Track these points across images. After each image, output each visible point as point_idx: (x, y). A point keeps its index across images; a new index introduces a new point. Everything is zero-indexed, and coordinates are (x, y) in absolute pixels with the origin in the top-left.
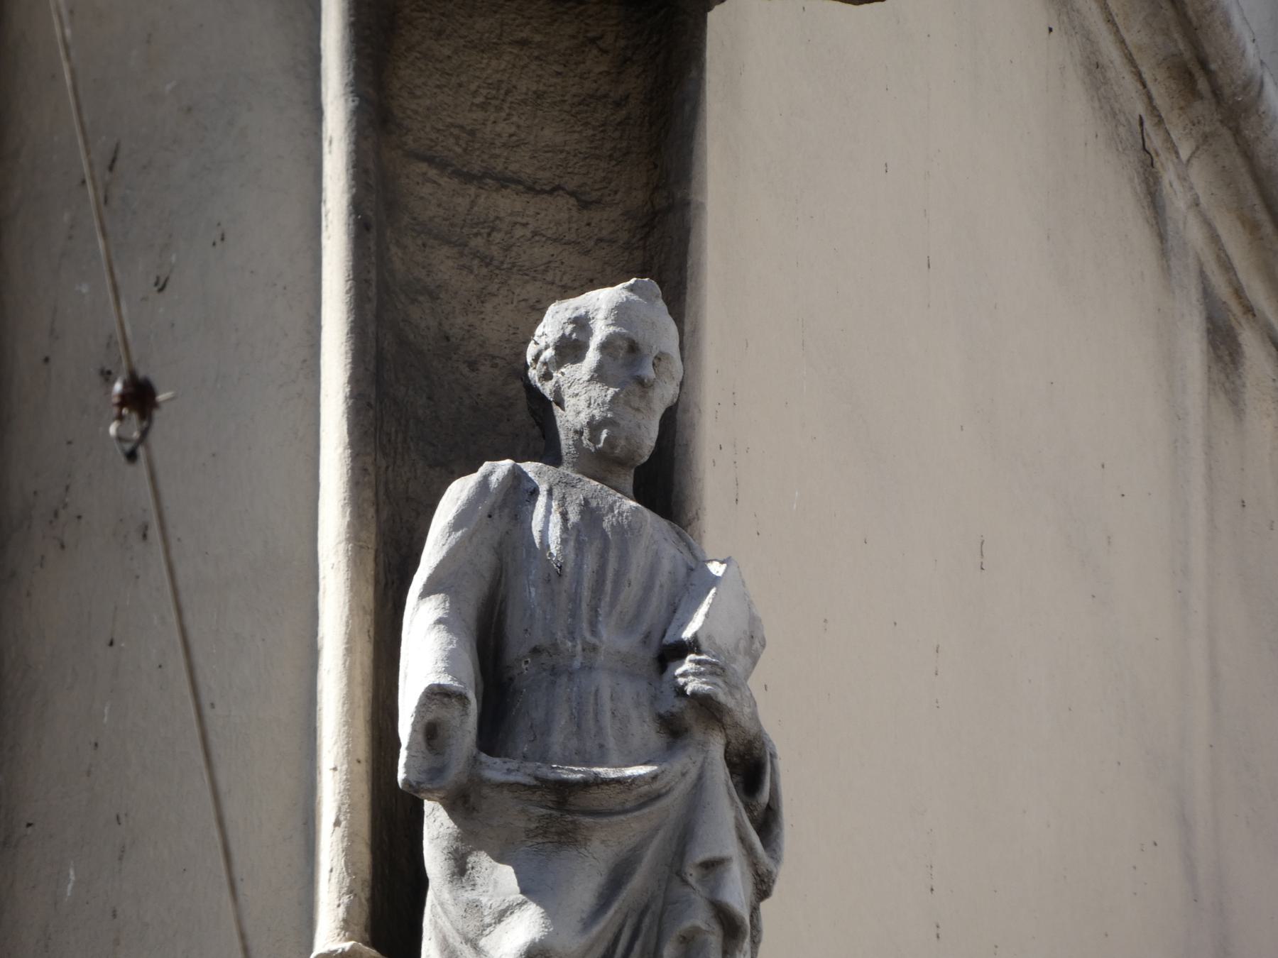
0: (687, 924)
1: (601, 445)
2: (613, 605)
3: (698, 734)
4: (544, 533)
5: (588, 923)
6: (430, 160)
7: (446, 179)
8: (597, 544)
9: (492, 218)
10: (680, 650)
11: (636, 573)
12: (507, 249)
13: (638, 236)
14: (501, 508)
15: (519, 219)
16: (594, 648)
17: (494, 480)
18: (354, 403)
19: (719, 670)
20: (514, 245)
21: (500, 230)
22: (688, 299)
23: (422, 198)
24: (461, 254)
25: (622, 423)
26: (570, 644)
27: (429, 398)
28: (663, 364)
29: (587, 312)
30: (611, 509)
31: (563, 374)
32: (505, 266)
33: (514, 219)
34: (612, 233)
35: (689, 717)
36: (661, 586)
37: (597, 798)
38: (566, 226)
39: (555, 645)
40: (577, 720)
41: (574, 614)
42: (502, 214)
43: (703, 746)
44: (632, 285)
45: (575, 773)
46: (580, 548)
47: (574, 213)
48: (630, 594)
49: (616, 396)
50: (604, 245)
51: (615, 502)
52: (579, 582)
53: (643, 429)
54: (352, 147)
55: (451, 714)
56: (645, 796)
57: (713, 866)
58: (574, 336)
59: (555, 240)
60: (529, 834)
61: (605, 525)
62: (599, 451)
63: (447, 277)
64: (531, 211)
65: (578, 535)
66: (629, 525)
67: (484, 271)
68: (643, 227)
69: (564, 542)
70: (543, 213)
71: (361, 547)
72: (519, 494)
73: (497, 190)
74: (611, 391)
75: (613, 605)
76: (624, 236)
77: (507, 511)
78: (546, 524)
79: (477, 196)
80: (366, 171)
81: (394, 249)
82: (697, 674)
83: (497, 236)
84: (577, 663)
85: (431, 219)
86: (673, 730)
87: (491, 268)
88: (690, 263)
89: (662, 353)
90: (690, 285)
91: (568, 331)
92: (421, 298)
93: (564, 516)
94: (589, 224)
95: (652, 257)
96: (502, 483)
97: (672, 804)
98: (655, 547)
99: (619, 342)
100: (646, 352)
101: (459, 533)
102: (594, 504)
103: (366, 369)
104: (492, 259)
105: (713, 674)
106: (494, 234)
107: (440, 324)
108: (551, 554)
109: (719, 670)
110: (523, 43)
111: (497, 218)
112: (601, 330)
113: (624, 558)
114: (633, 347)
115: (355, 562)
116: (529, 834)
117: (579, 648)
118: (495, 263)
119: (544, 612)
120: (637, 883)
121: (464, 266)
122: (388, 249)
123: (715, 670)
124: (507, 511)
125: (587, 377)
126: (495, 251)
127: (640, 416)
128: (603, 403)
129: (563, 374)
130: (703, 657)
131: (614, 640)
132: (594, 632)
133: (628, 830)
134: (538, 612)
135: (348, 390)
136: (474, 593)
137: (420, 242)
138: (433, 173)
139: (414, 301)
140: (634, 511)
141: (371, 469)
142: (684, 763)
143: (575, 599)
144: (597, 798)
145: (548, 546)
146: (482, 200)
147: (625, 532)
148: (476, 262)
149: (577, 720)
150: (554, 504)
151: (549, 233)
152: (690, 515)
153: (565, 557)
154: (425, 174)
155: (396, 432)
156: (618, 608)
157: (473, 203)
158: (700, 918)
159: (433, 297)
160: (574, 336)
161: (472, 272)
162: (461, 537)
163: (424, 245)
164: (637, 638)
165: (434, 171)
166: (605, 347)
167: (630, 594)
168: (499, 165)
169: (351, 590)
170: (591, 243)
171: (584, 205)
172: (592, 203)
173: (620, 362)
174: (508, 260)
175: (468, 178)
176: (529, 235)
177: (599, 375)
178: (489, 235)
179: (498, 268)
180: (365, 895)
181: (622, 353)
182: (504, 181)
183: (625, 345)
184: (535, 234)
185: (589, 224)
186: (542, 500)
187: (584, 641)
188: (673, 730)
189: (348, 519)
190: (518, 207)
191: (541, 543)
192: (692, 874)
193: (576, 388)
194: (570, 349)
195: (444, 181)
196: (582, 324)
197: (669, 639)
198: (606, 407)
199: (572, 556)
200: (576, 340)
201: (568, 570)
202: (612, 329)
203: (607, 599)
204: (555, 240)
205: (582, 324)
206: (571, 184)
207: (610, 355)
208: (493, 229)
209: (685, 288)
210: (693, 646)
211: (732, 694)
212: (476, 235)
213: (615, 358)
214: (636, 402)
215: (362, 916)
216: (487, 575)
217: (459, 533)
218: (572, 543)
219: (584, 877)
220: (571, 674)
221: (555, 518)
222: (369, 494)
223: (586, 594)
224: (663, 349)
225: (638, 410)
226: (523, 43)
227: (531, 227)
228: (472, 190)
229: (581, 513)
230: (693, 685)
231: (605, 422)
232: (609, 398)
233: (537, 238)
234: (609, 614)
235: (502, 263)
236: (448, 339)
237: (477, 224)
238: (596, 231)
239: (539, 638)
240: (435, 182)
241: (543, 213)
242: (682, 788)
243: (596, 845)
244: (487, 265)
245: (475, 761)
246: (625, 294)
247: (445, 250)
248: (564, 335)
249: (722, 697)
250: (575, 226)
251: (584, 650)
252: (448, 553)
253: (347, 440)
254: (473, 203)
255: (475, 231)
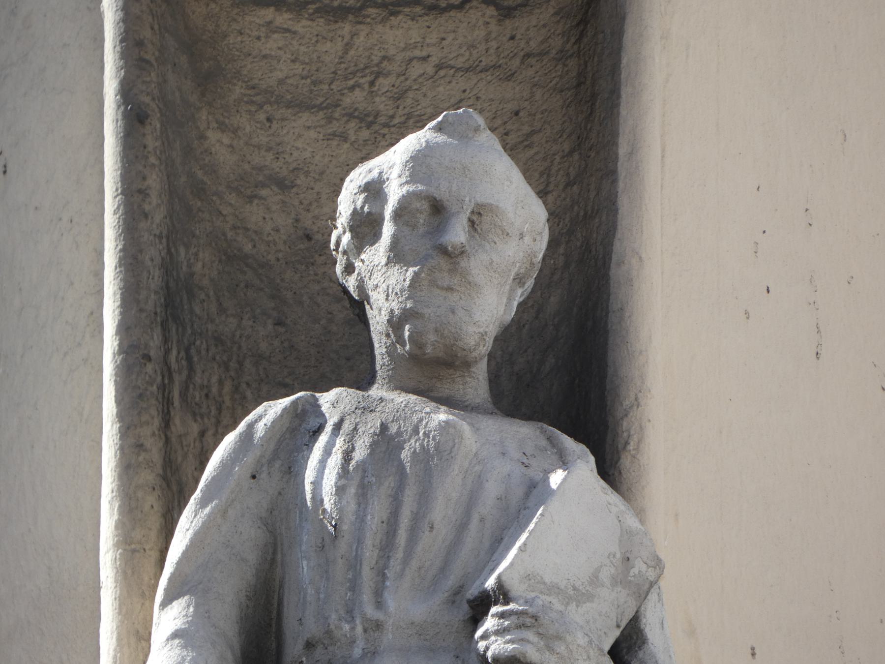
1: (408, 347)
2: (406, 562)
4: (317, 484)
7: (304, 22)
8: (390, 482)
9: (376, 59)
10: (480, 607)
11: (442, 512)
12: (399, 97)
13: (573, 40)
14: (270, 462)
15: (417, 53)
16: (378, 626)
17: (260, 429)
18: (124, 360)
19: (528, 621)
20: (410, 88)
21: (387, 75)
22: (623, 112)
23: (265, 57)
24: (330, 119)
25: (426, 311)
26: (347, 627)
27: (279, 323)
28: (486, 218)
29: (380, 173)
30: (416, 431)
31: (363, 261)
32: (396, 121)
33: (409, 54)
34: (542, 42)
36: (482, 520)
38: (482, 47)
39: (329, 633)
41: (354, 586)
42: (392, 52)
44: (440, 123)
46: (364, 493)
47: (493, 27)
48: (432, 545)
49: (416, 275)
50: (533, 61)
51: (421, 420)
52: (360, 541)
53: (461, 313)
54: (120, 14)
58: (366, 209)
59: (467, 70)
61: (405, 455)
62: (409, 353)
63: (307, 155)
64: (433, 38)
65: (363, 478)
66: (437, 448)
67: (365, 134)
68: (578, 24)
69: (340, 490)
70: (450, 37)
71: (134, 551)
73: (383, 21)
74: (411, 270)
75: (406, 562)
76: (557, 43)
77: (278, 464)
79: (353, 35)
80: (140, 44)
81: (213, 136)
82: (499, 632)
83: (384, 83)
84: (357, 652)
85: (281, 82)
87: (376, 127)
88: (624, 61)
89: (478, 205)
90: (626, 92)
91: (359, 204)
92: (264, 192)
93: (347, 456)
94: (512, 38)
95: (586, 63)
96: (271, 429)
98: (478, 468)
99: (417, 205)
100: (454, 208)
101: (207, 510)
102: (393, 429)
103: (141, 310)
104: (377, 116)
105: (520, 627)
106: (381, 80)
107: (297, 221)
108: (324, 511)
109: (528, 621)
111: (384, 58)
112: (395, 192)
113: (425, 497)
114: (438, 209)
115: (124, 573)
117: (359, 629)
118: (382, 119)
119: (318, 592)
121: (334, 135)
122: (202, 137)
124: (278, 464)
125: (384, 261)
126: (382, 104)
127: (455, 297)
128: (402, 291)
129: (363, 261)
130: (512, 606)
132: (379, 604)
134: (310, 591)
135: (116, 343)
136: (231, 589)
137: (262, 116)
139: (251, 198)
140: (445, 427)
143: (355, 564)
145: (322, 501)
146: (360, 40)
147: (433, 460)
148: (352, 124)
150: (340, 442)
151: (459, 63)
152: (626, 403)
153: (340, 511)
154: (270, 23)
155: (221, 382)
156: (414, 564)
157: (348, 47)
159: (284, 185)
160: (366, 209)
161: (346, 139)
162: (209, 516)
163: (269, 120)
164: (441, 596)
165: (287, 16)
166: (398, 215)
169: (120, 613)
170: (516, 62)
172: (515, 9)
173: (422, 230)
174: (400, 112)
176: (430, 70)
178: (372, 83)
179: (386, 125)
181: (422, 219)
183: (425, 206)
184: (439, 67)
185: (512, 38)
186: (323, 439)
187: (365, 620)
189: (116, 517)
190: (415, 36)
191: (313, 498)
193: (377, 278)
194: (365, 228)
195: (303, 26)
196: (374, 190)
197: (472, 592)
198: (406, 294)
199: (353, 506)
200: (369, 213)
201: (345, 527)
202: (405, 189)
203: (399, 554)
204: (467, 70)
205: (374, 190)
207: (407, 224)
208: (378, 75)
209: (619, 97)
210: (502, 594)
211: (551, 649)
212: (352, 88)
213: (414, 227)
214: (445, 279)
216: (252, 557)
217: (207, 510)
218: (352, 490)
223: (370, 555)
224: (481, 199)
225: (450, 289)
227: (434, 60)
228: (346, 28)
229: (373, 446)
232: (408, 282)
233: (442, 73)
234: (401, 575)
235: (392, 117)
236: (309, 238)
237: (354, 74)
238: (522, 44)
239: (312, 628)
240: (287, 30)
241: (450, 37)
244: (369, 126)
246: (428, 133)
247: (306, 118)
248: (355, 209)
250: (494, 44)
251: (365, 631)
252: (192, 541)
253: (115, 411)
254: (348, 47)
255: (351, 83)
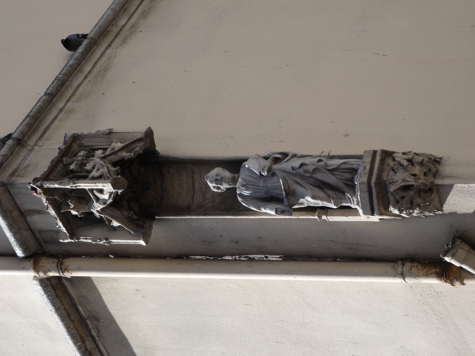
0: (303, 173)
3: (273, 171)
5: (307, 189)
6: (193, 198)
8: (247, 185)
35: (271, 172)
37: (287, 189)
40: (275, 189)
41: (259, 189)
43: (275, 169)
45: (284, 193)
46: (249, 188)
55: (279, 210)
56: (284, 180)
57: (293, 168)
60: (295, 197)
69: (248, 191)
72: (241, 195)
78: (246, 193)
86: (273, 174)
97: (285, 175)
110: (171, 182)
112: (214, 185)
113: (249, 181)
116: (295, 197)
120: (298, 180)
123: (263, 170)
131: (261, 183)
132: (261, 186)
133: (290, 182)
136: (260, 203)
138: (195, 198)
141: (243, 212)
142: (278, 173)
143: (257, 189)
144: (287, 189)
147: (244, 180)
149: (275, 189)
158: (301, 171)
159: (214, 198)
166: (217, 184)
167: (254, 180)
168: (191, 186)
171: (194, 172)
175: (194, 191)
177: (222, 185)
180: (308, 213)
182: (193, 185)
188: (273, 174)
192: (295, 172)
194: (218, 188)
196: (214, 187)
205: (214, 187)
206: (191, 174)
215: (312, 213)
219: (300, 190)
220: (268, 190)
221: (245, 191)
222: (247, 213)
226: (171, 182)
228: (196, 190)
230: (266, 173)
231: (228, 183)
239: (264, 194)
242: (283, 174)
243: (294, 187)
245: (285, 206)
249: (267, 169)
